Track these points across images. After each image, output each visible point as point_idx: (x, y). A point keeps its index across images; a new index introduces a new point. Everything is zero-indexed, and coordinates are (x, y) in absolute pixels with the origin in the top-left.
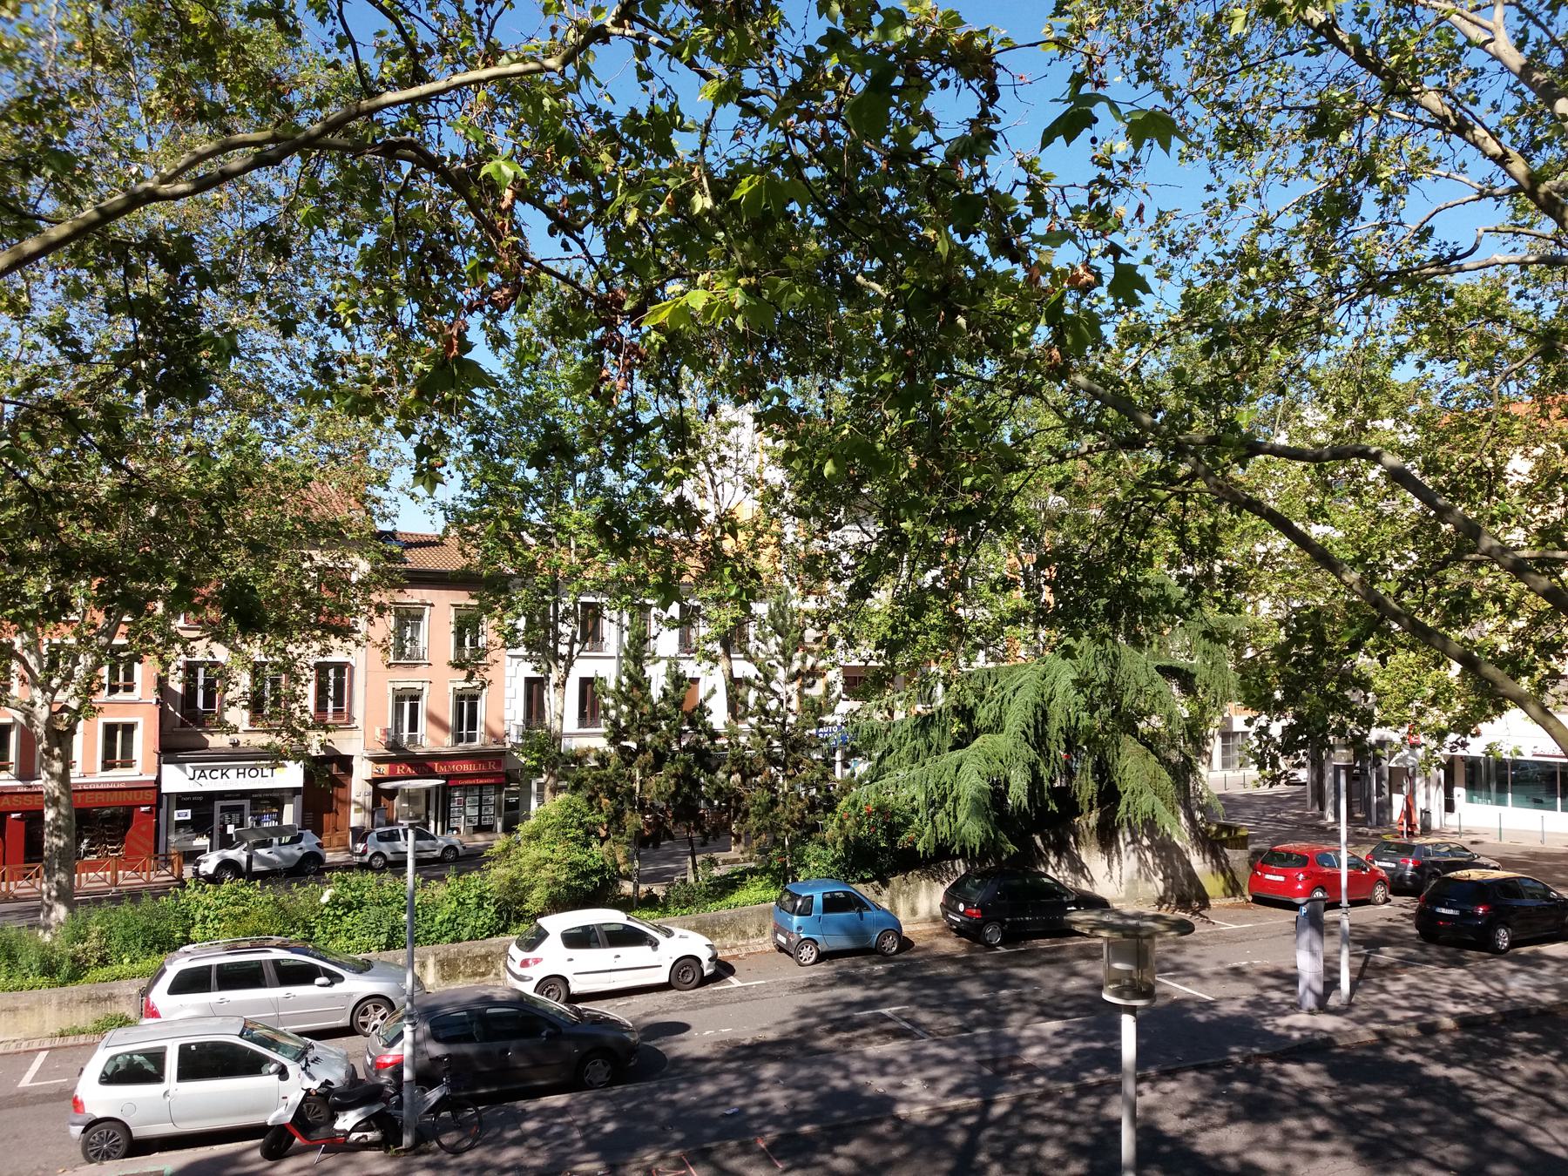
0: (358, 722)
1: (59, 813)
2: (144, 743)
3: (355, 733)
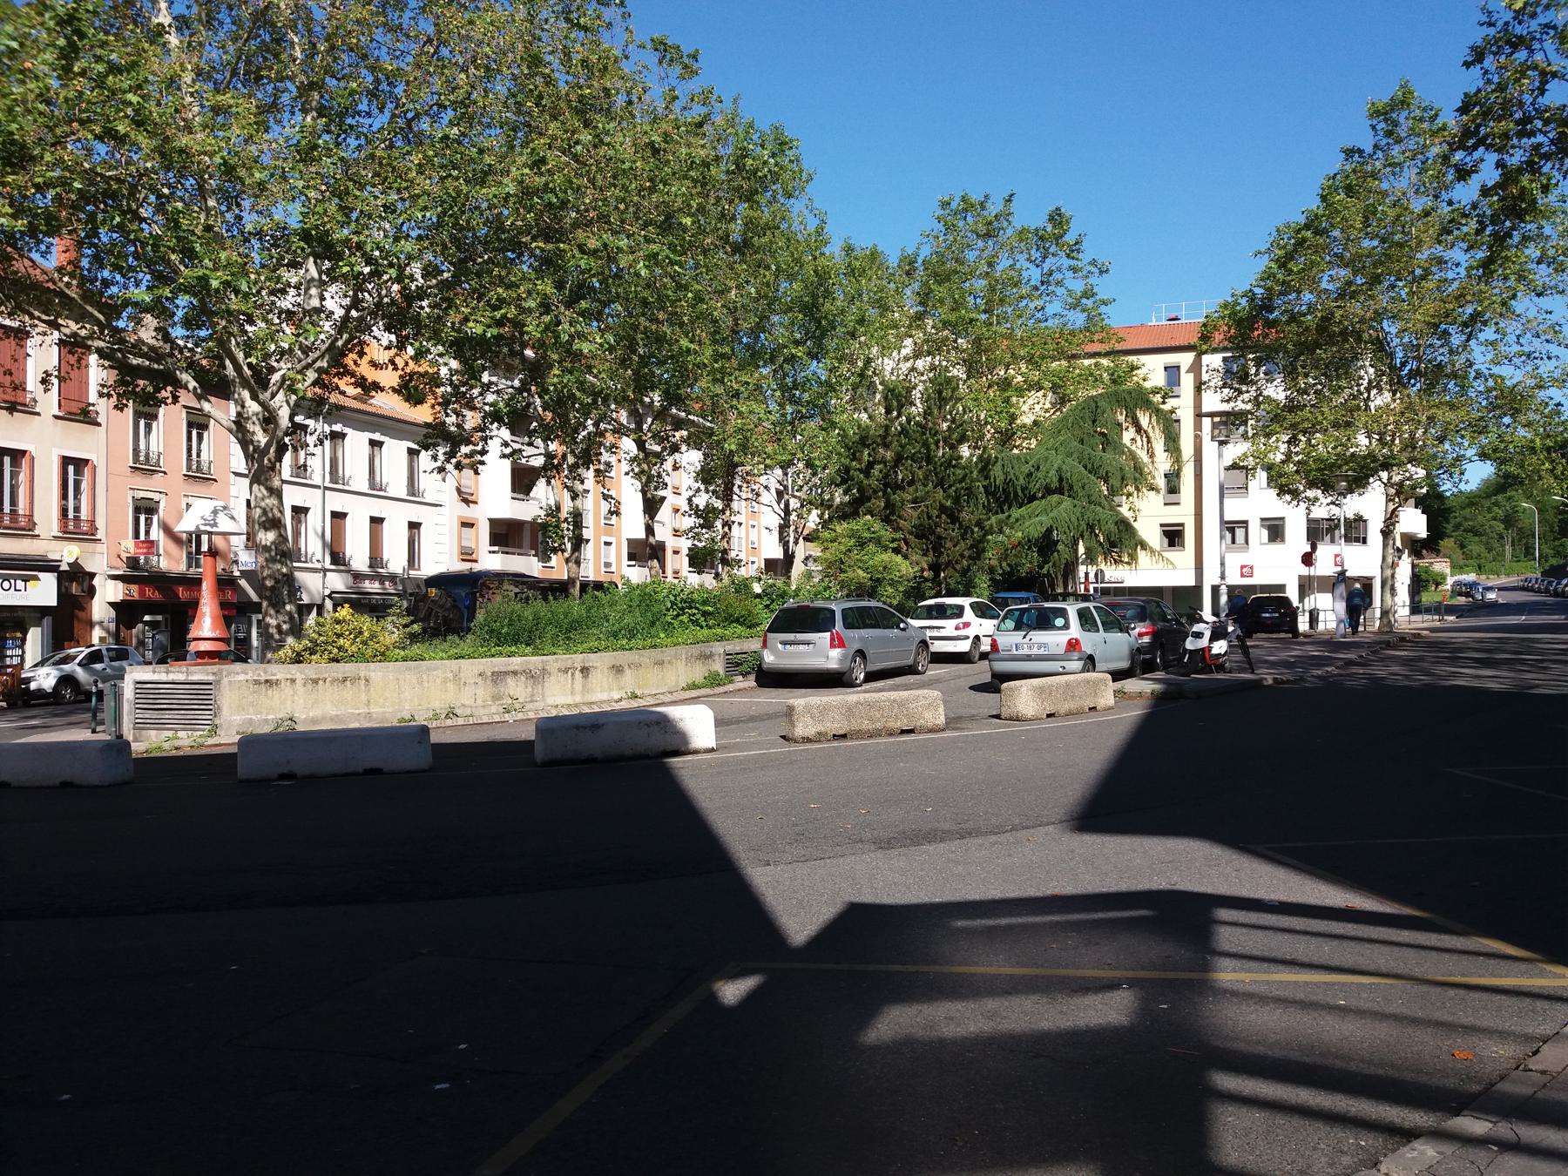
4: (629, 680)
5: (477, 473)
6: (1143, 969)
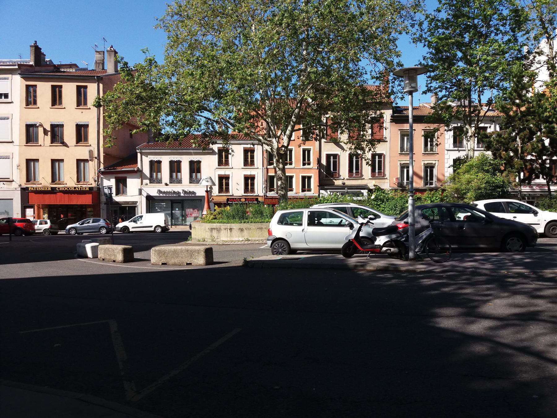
0: (387, 176)
1: (282, 182)
2: (314, 183)
3: (386, 181)
4: (246, 235)
5: (37, 51)
6: (35, 133)
